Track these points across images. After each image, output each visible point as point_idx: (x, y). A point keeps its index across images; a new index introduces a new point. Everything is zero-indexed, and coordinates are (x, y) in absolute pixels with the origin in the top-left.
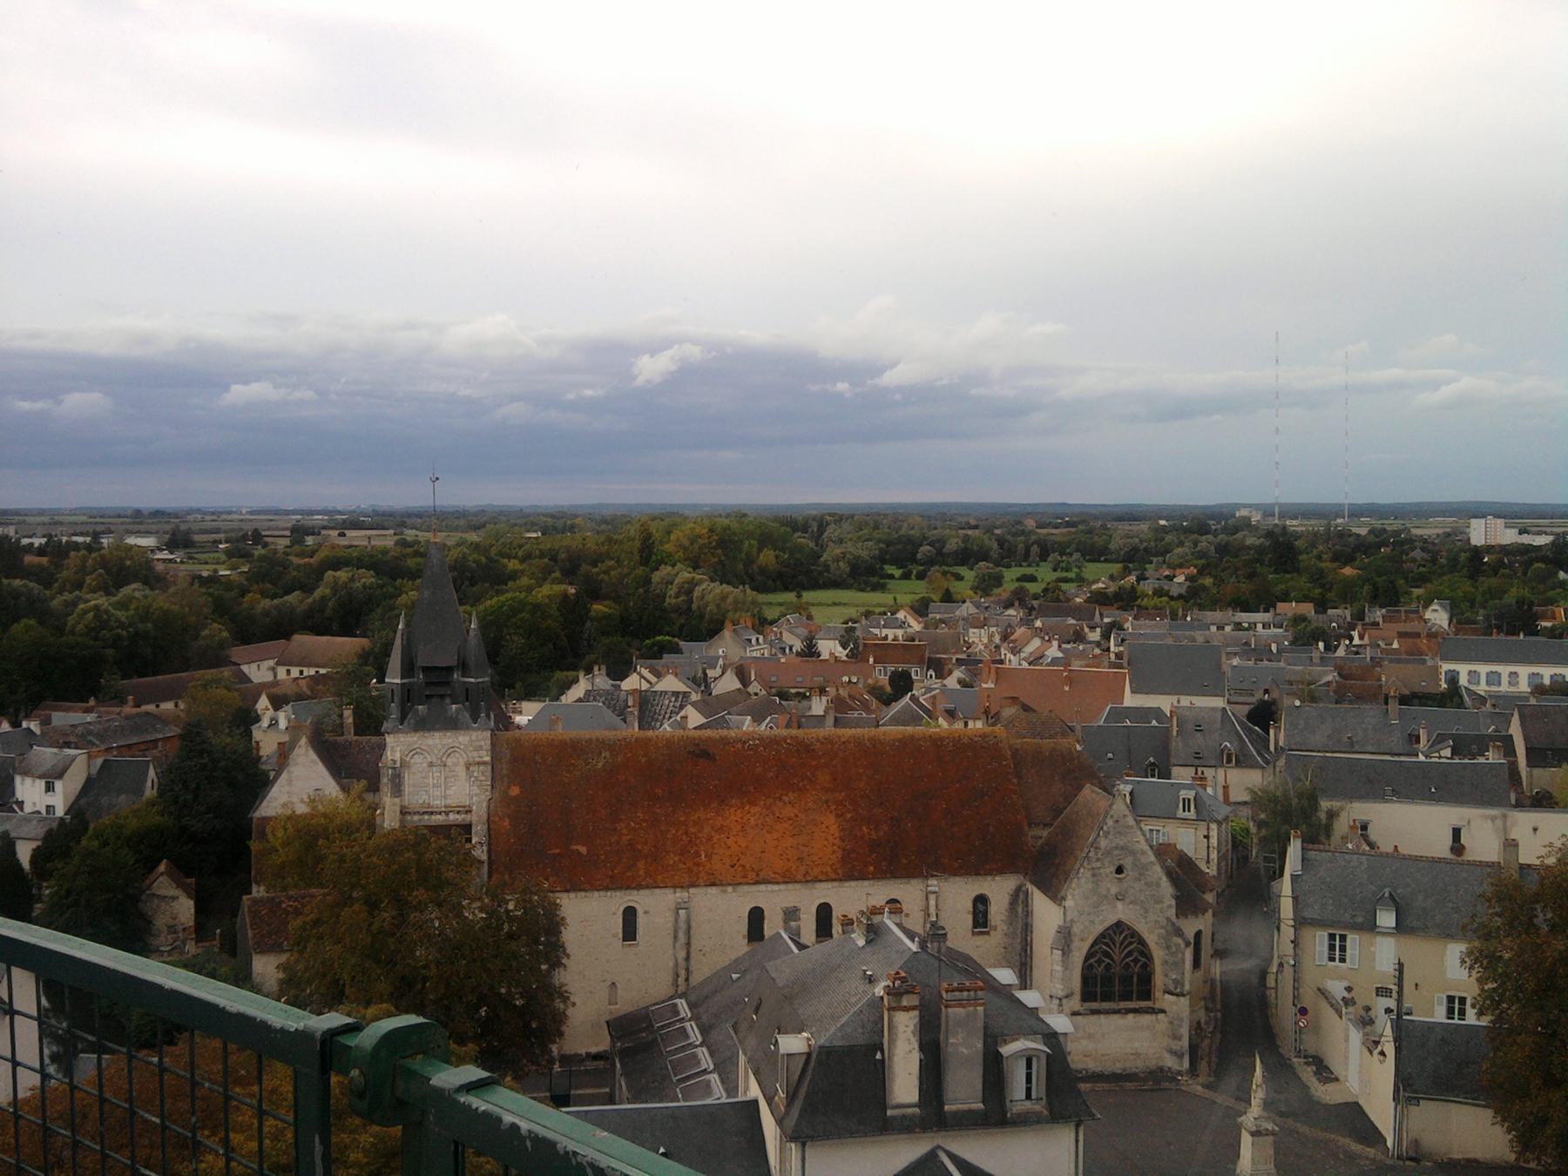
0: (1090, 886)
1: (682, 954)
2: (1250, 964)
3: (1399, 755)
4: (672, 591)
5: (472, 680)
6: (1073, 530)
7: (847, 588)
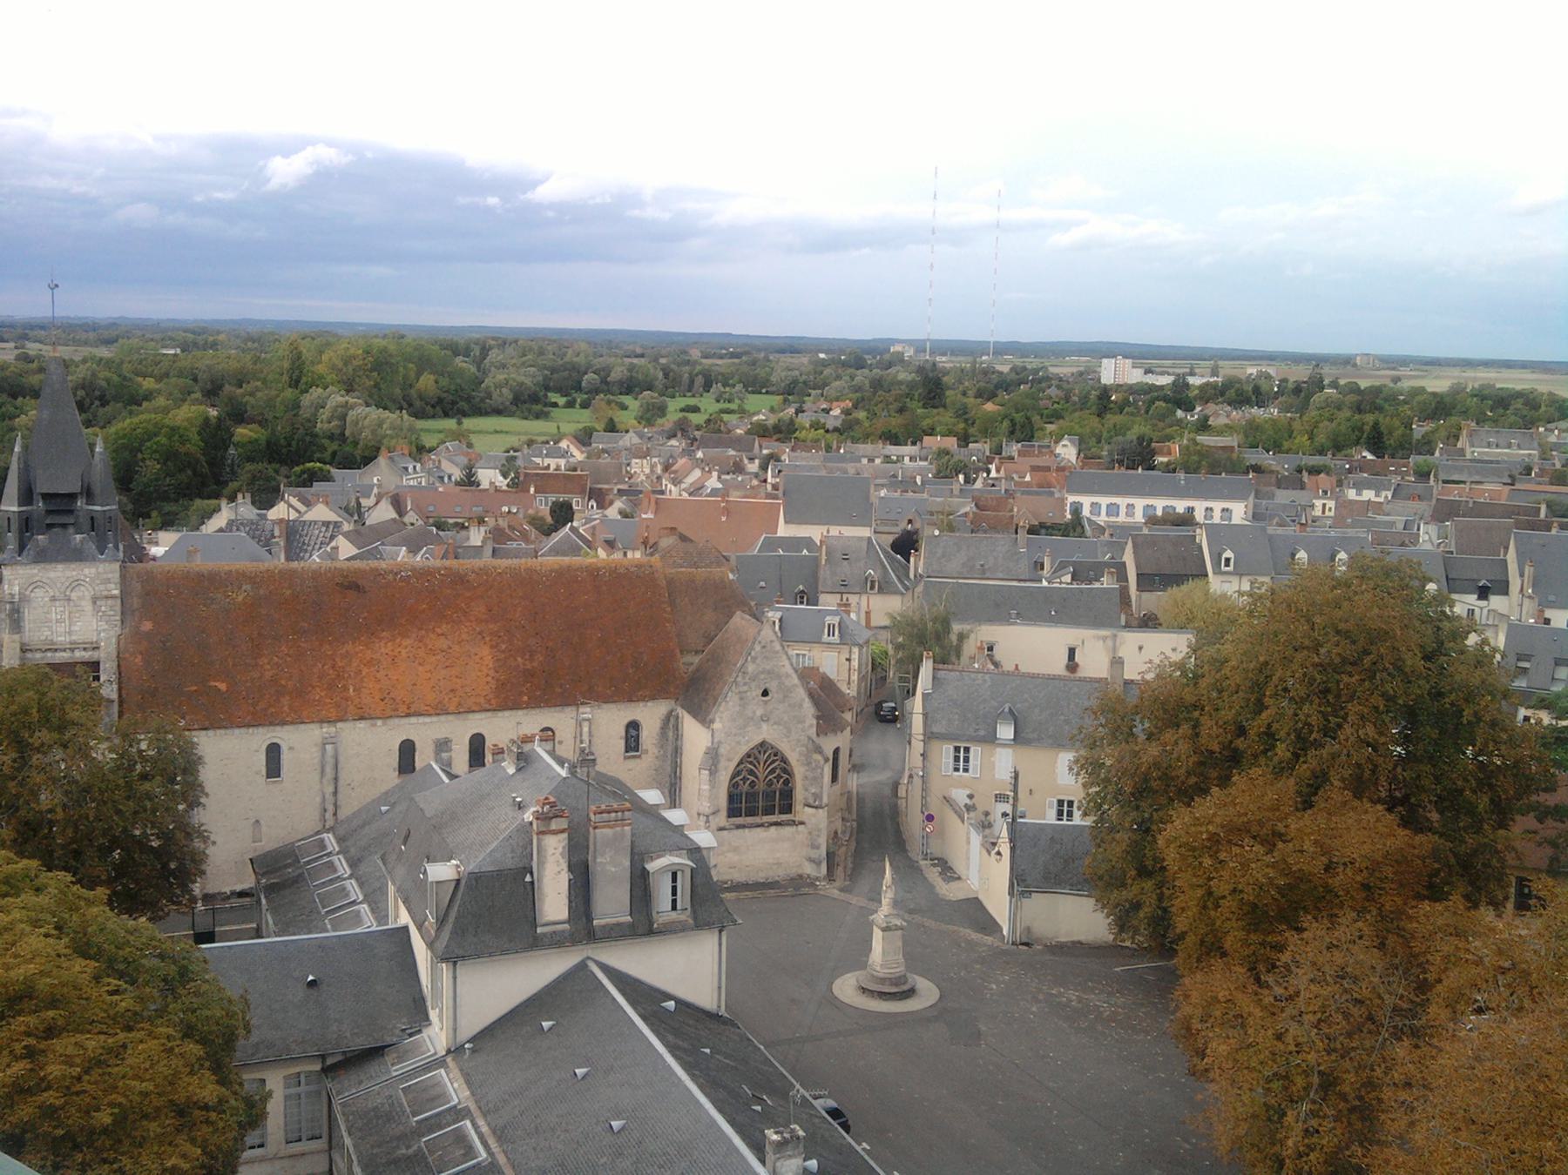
0: (737, 708)
1: (331, 789)
2: (884, 776)
3: (1025, 581)
4: (324, 414)
6: (736, 361)
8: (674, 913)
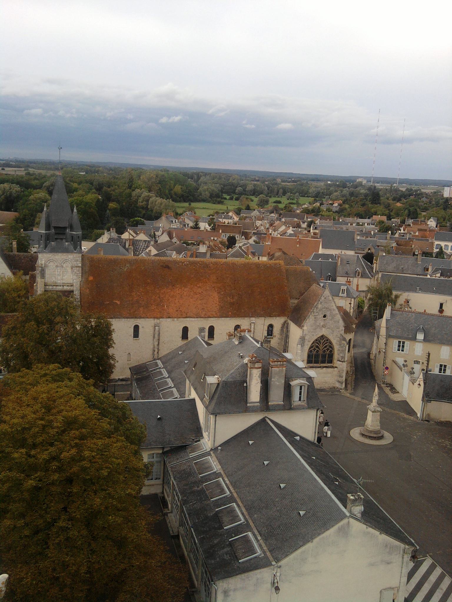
0: (313, 322)
1: (156, 343)
2: (364, 350)
3: (420, 275)
4: (140, 200)
5: (75, 233)
6: (295, 184)
7: (209, 202)
8: (300, 402)
